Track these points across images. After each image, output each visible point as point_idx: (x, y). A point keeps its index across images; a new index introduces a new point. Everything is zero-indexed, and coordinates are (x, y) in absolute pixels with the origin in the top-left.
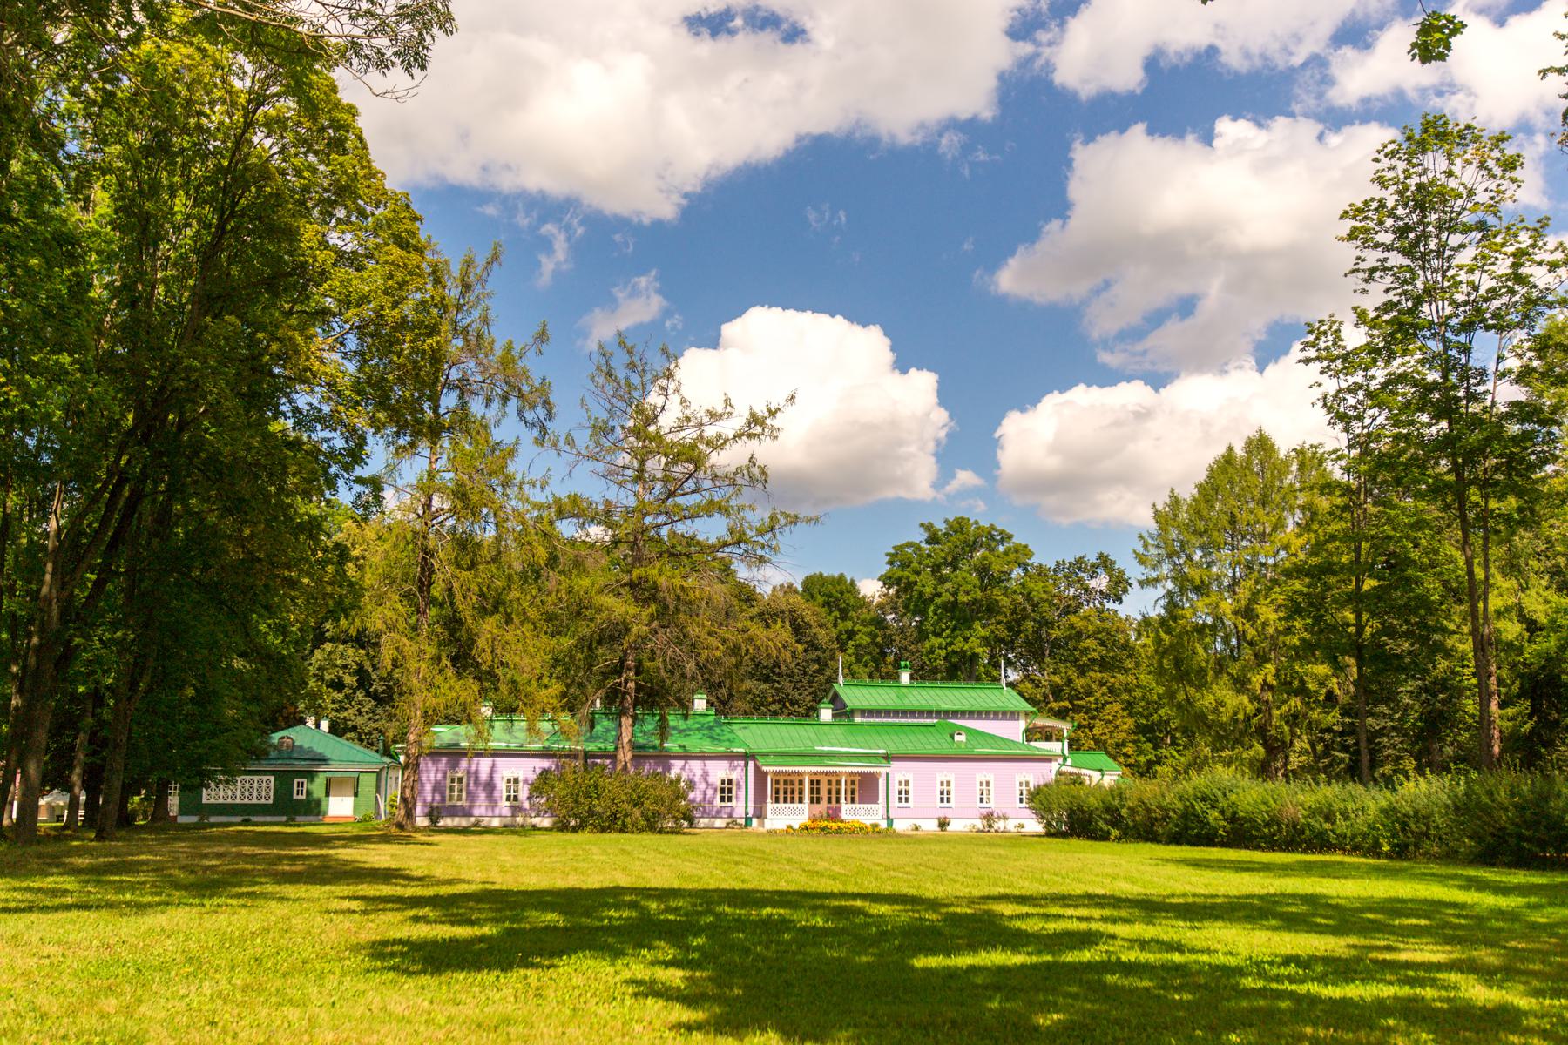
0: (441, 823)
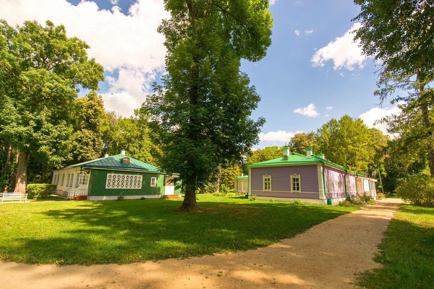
0: (115, 198)
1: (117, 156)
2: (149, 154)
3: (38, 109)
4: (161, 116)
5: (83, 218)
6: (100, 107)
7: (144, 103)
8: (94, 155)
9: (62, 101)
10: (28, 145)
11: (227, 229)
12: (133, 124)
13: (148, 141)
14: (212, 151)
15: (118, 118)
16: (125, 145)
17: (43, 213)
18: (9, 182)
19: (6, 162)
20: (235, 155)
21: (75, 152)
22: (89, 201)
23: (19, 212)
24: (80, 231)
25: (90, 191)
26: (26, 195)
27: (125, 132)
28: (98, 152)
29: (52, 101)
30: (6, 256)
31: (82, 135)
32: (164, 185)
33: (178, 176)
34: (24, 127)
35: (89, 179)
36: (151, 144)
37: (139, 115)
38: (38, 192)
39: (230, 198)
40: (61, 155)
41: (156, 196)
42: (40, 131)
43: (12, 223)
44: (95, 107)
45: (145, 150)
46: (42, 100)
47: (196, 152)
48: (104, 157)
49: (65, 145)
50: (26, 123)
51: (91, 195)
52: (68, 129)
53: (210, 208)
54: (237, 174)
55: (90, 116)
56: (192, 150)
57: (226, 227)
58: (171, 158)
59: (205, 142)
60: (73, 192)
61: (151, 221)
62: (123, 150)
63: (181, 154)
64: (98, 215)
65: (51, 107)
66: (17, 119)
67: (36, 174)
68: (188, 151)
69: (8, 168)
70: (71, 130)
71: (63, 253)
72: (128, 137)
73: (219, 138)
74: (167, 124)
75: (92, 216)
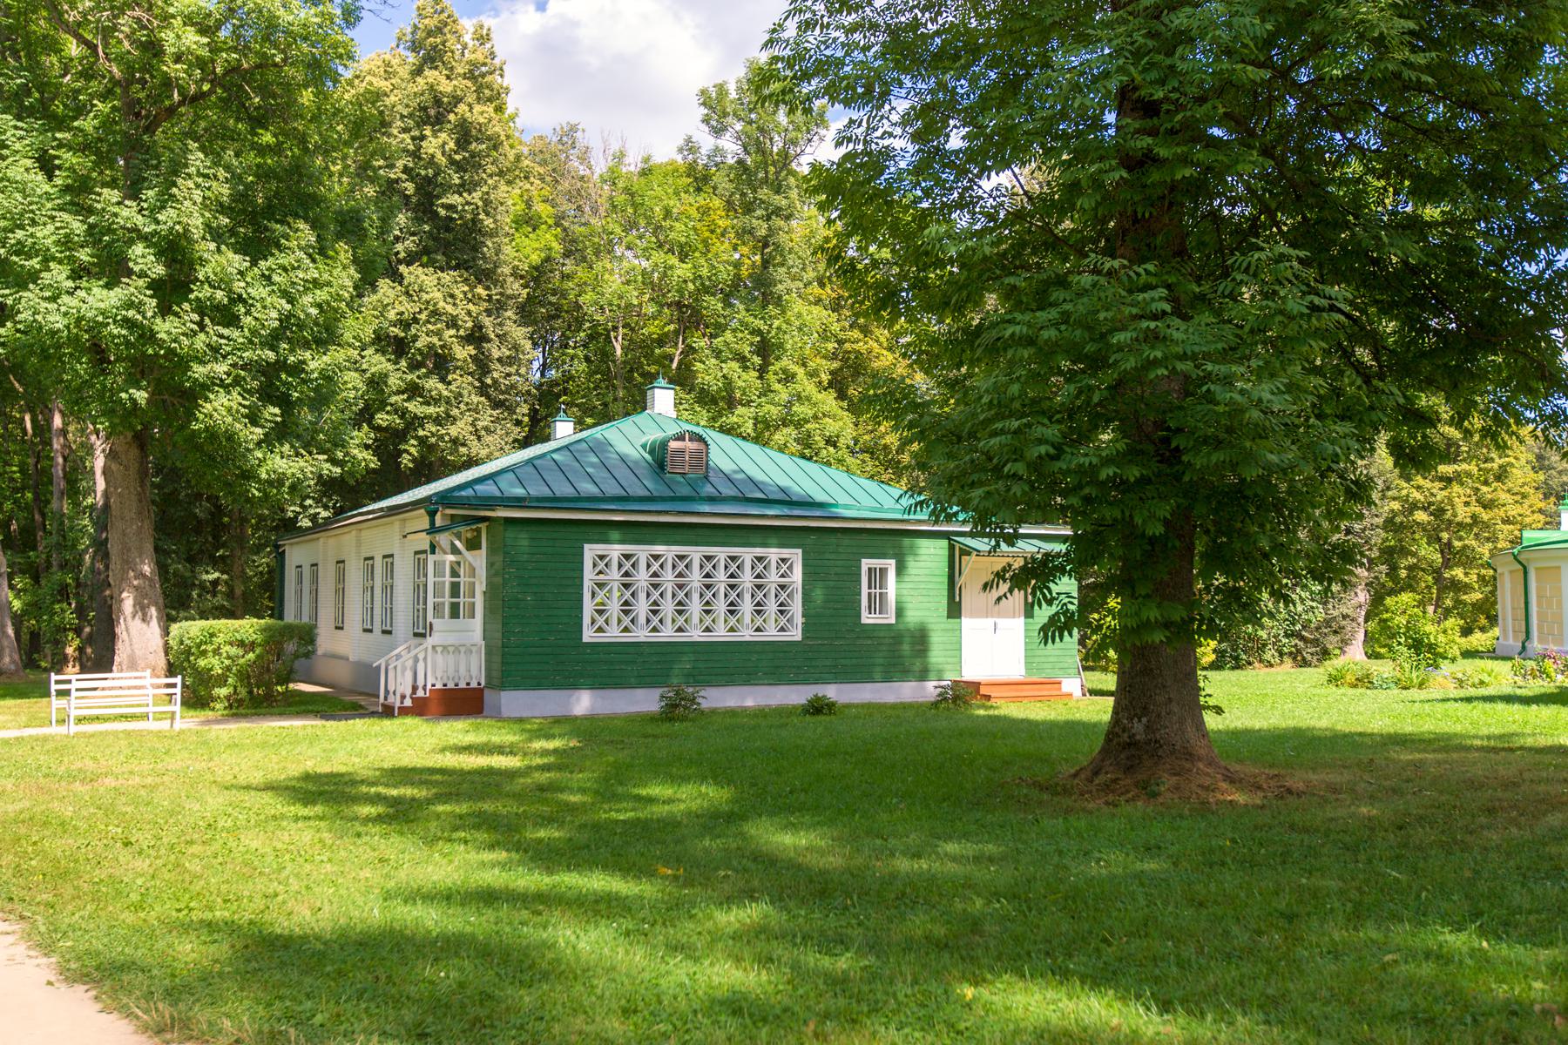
0: (647, 701)
1: (626, 424)
2: (829, 400)
3: (156, 167)
4: (902, 106)
5: (483, 821)
6: (490, 109)
7: (777, 28)
8: (486, 429)
9: (274, 96)
10: (141, 396)
11: (1483, 932)
12: (701, 200)
13: (816, 310)
14: (1318, 334)
15: (600, 166)
16: (668, 350)
17: (270, 787)
18: (81, 612)
19: (48, 502)
20: (1511, 351)
21: (382, 419)
22: (499, 717)
23: (158, 780)
24: (488, 897)
25: (497, 659)
26: (174, 685)
27: (658, 257)
28: (511, 410)
29: (225, 104)
30: (157, 1010)
31: (408, 308)
32: (954, 610)
33: (1061, 548)
34: (108, 286)
35: (481, 587)
36: (835, 327)
37: (739, 126)
38: (228, 669)
39: (1469, 700)
40: (309, 443)
41: (906, 691)
42: (186, 306)
43: (143, 838)
44: (462, 108)
45: (800, 371)
46: (171, 111)
47: (1183, 357)
48: (547, 439)
49: (327, 378)
50: (113, 268)
51: (503, 686)
52: (326, 276)
53: (1313, 777)
54: (1513, 511)
55: (436, 175)
56: (1154, 338)
57: (1478, 914)
58: (1000, 417)
59: (1253, 273)
60: (403, 670)
61: (904, 854)
62: (661, 382)
63: (1070, 377)
64: (567, 804)
65: (223, 149)
66: (67, 243)
67: (200, 563)
68: (1120, 349)
69: (62, 532)
70: (345, 278)
71: (430, 1019)
72: (681, 291)
73: (1371, 224)
74: (952, 165)
75: (533, 809)
